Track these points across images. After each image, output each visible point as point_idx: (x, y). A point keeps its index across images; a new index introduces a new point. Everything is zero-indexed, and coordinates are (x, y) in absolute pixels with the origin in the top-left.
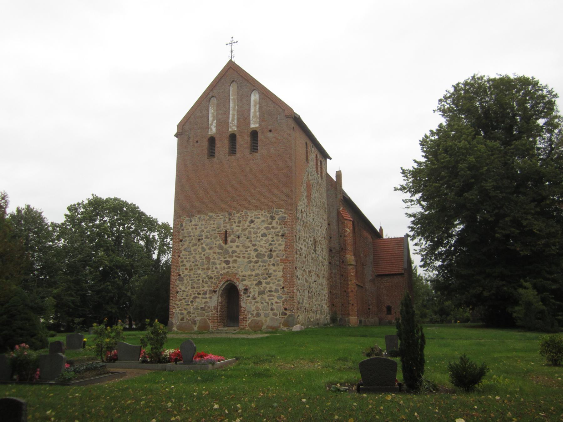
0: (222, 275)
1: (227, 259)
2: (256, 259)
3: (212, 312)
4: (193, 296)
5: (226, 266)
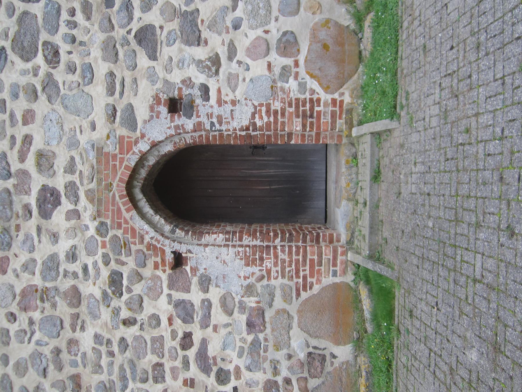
0: (102, 224)
1: (32, 200)
2: (40, 60)
3: (269, 272)
4: (194, 371)
5: (66, 205)
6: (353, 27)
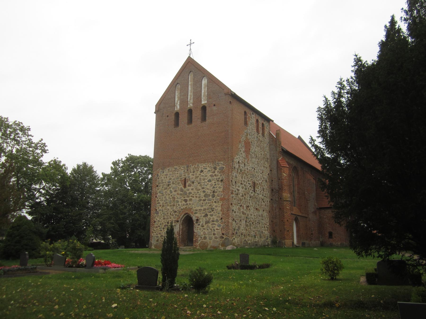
1: (186, 198)
2: (204, 198)
5: (185, 203)
6: (208, 249)
